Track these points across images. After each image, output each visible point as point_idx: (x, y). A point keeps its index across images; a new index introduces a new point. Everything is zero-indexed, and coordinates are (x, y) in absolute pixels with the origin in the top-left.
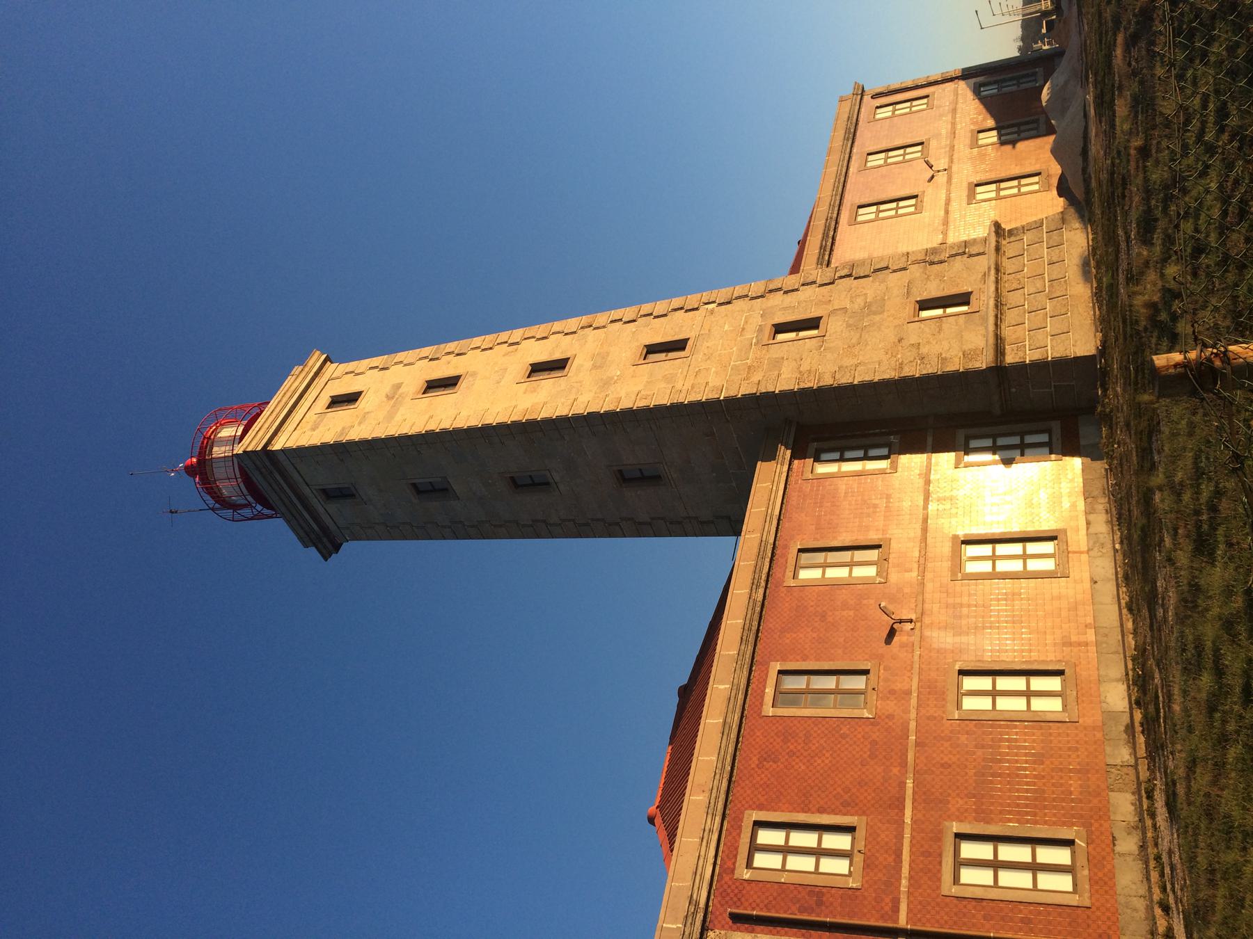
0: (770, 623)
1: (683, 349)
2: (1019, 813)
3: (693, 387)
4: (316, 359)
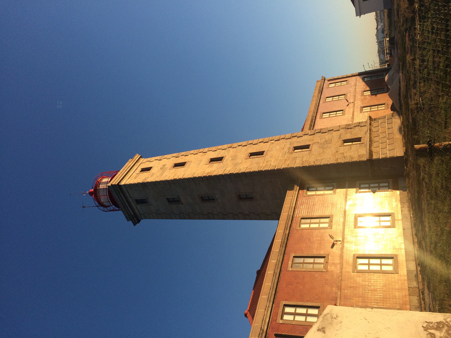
0: (291, 241)
1: (263, 154)
2: (377, 303)
3: (266, 165)
4: (137, 157)
